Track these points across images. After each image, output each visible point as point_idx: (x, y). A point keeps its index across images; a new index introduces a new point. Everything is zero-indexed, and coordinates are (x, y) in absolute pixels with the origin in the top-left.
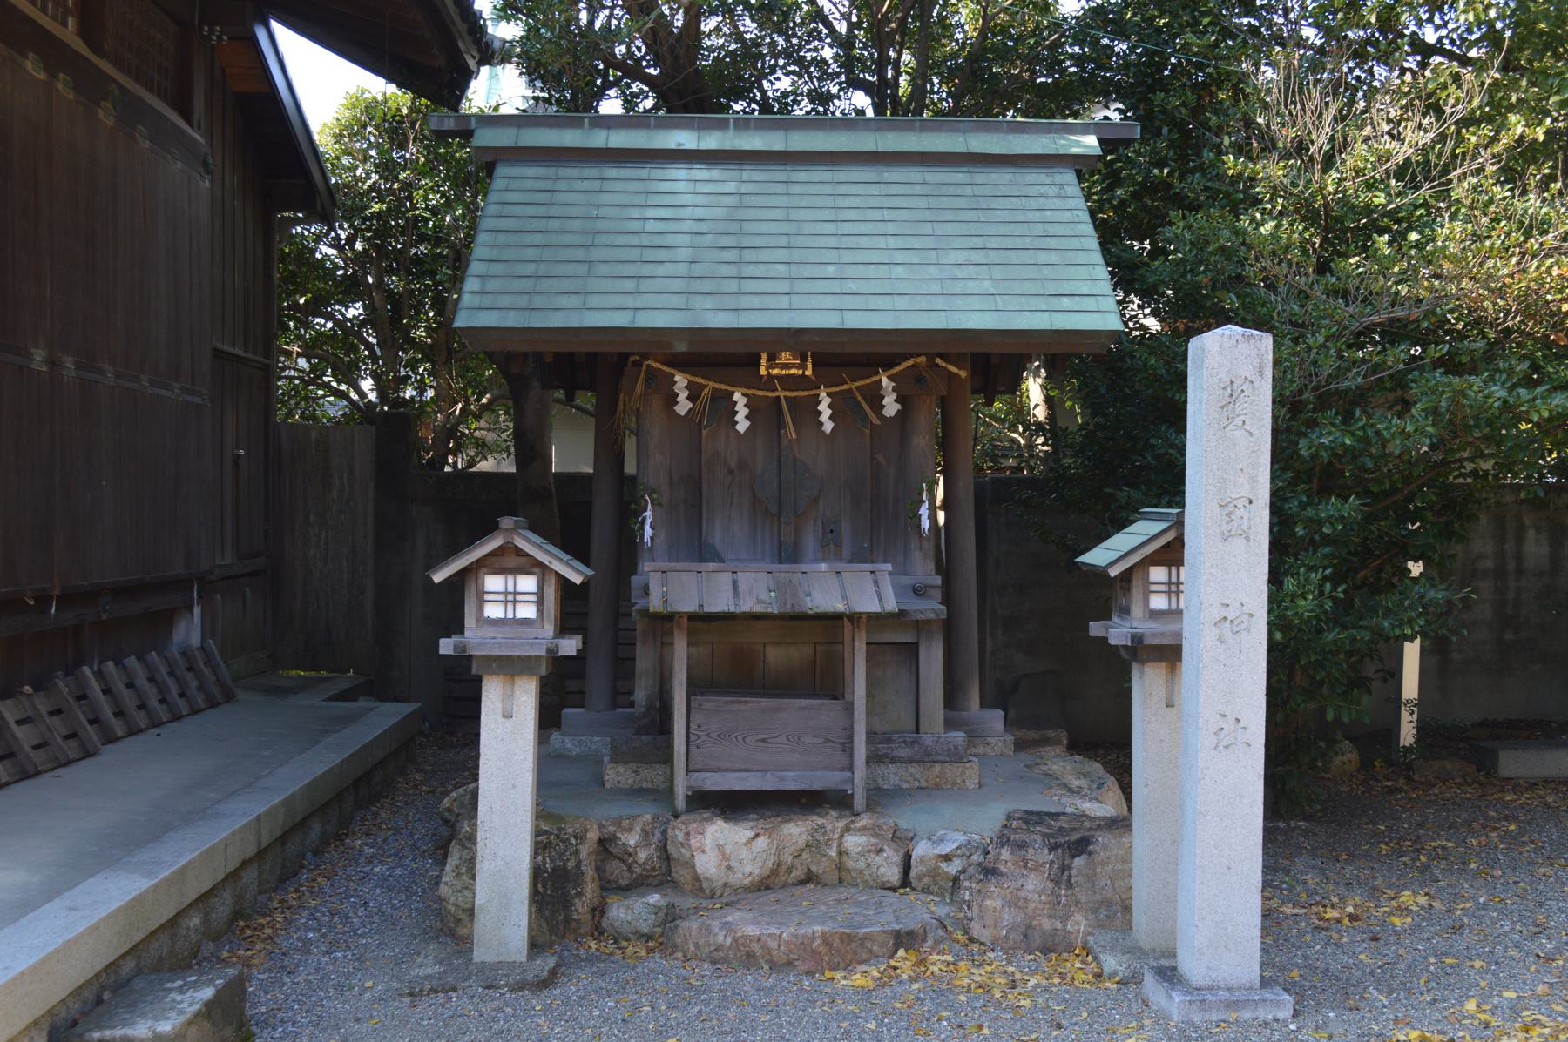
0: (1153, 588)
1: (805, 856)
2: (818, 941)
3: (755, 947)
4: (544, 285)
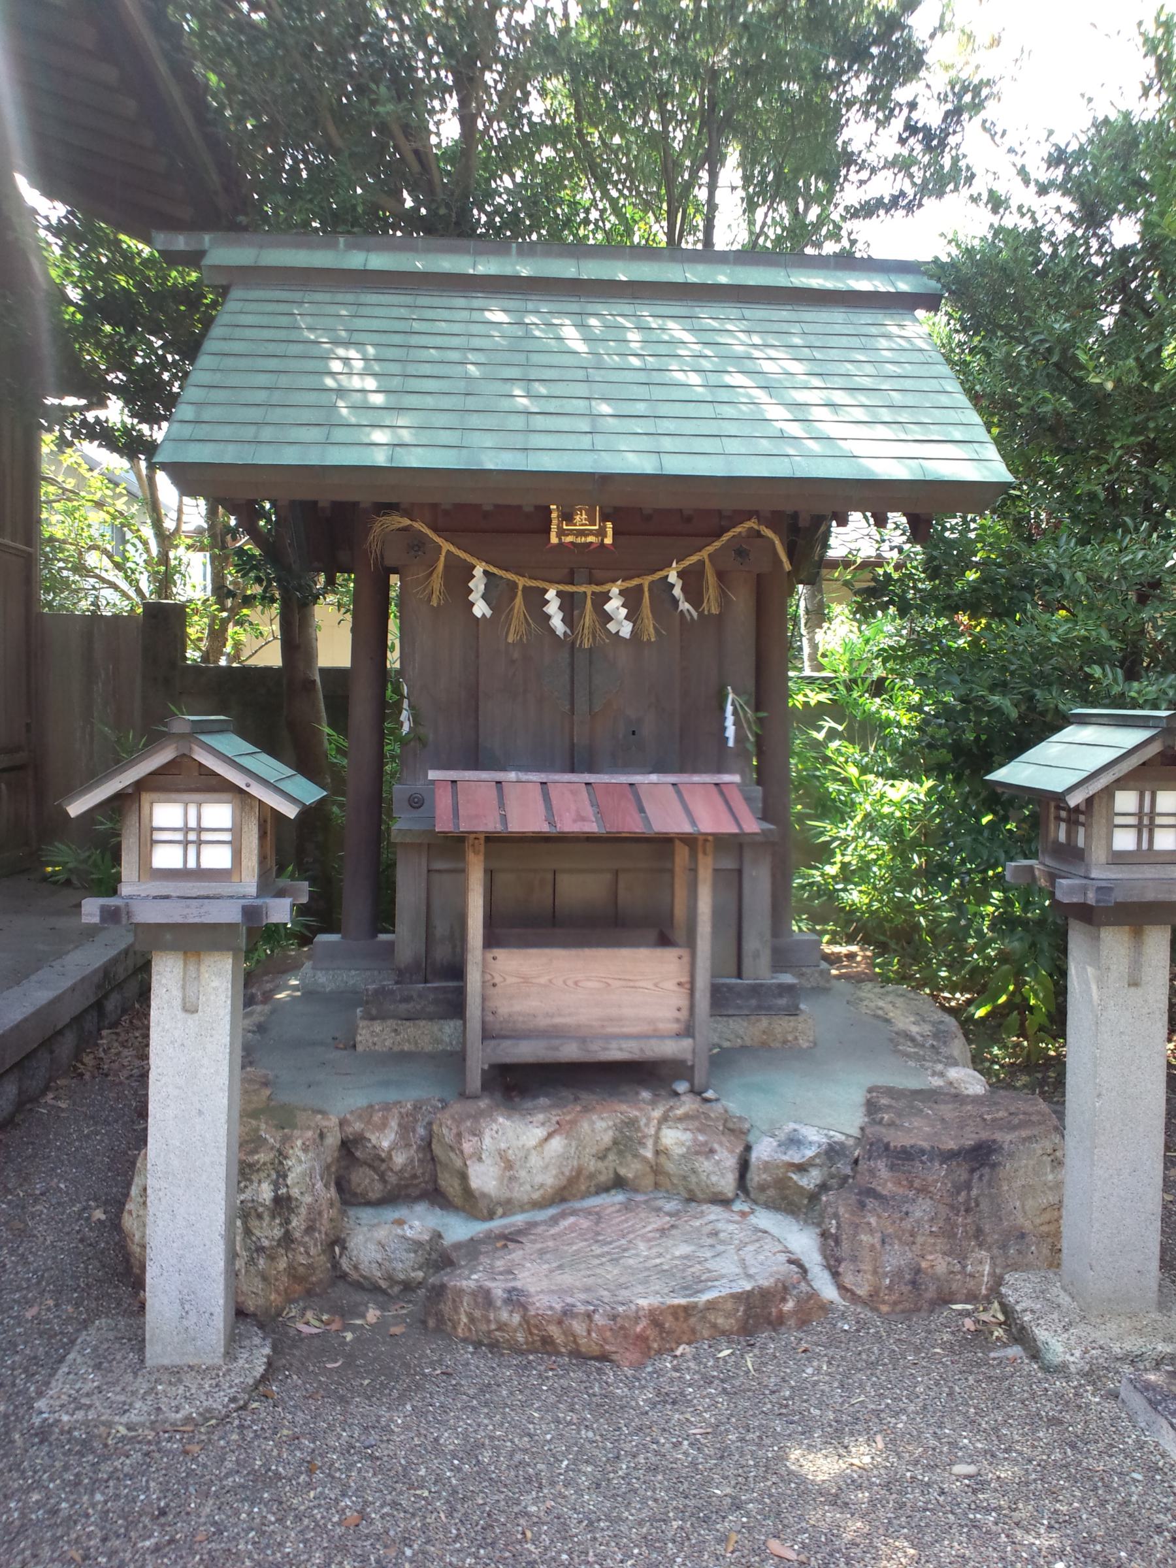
0: (1118, 820)
1: (611, 1157)
2: (643, 1323)
3: (554, 1331)
4: (276, 415)
